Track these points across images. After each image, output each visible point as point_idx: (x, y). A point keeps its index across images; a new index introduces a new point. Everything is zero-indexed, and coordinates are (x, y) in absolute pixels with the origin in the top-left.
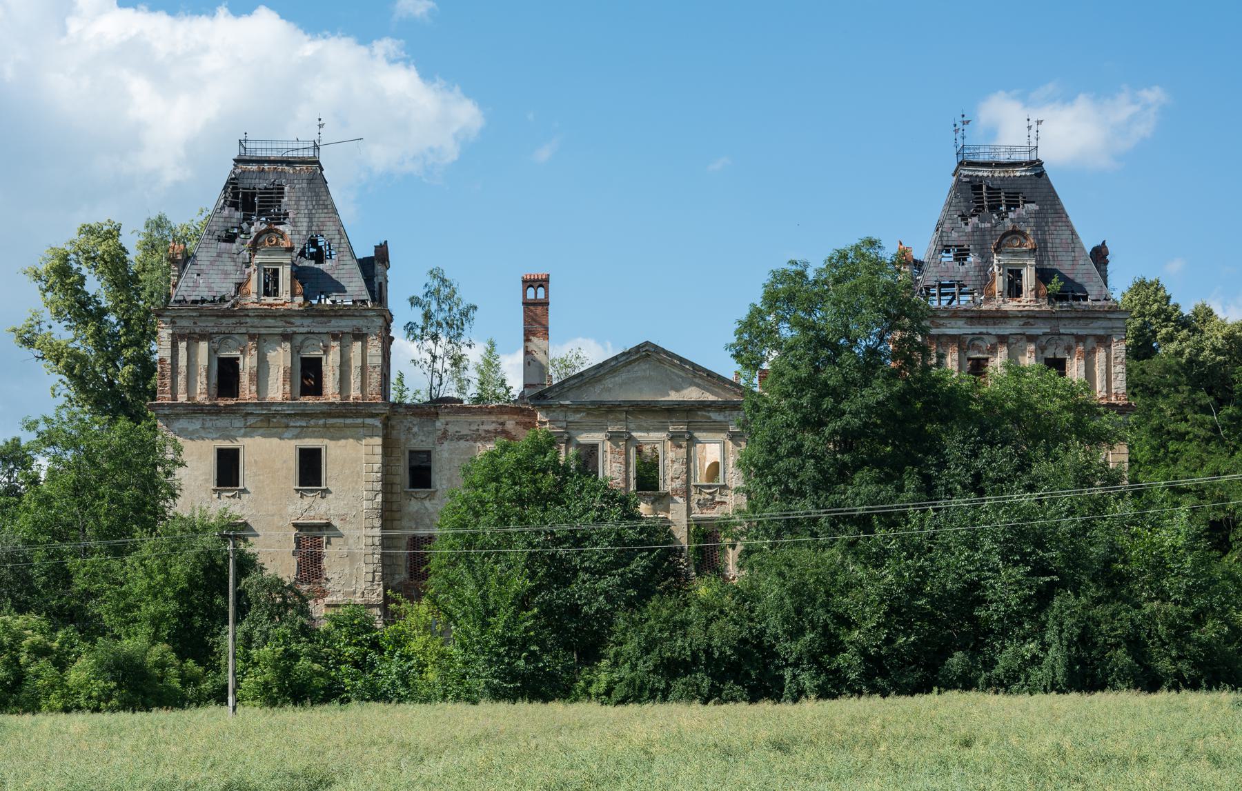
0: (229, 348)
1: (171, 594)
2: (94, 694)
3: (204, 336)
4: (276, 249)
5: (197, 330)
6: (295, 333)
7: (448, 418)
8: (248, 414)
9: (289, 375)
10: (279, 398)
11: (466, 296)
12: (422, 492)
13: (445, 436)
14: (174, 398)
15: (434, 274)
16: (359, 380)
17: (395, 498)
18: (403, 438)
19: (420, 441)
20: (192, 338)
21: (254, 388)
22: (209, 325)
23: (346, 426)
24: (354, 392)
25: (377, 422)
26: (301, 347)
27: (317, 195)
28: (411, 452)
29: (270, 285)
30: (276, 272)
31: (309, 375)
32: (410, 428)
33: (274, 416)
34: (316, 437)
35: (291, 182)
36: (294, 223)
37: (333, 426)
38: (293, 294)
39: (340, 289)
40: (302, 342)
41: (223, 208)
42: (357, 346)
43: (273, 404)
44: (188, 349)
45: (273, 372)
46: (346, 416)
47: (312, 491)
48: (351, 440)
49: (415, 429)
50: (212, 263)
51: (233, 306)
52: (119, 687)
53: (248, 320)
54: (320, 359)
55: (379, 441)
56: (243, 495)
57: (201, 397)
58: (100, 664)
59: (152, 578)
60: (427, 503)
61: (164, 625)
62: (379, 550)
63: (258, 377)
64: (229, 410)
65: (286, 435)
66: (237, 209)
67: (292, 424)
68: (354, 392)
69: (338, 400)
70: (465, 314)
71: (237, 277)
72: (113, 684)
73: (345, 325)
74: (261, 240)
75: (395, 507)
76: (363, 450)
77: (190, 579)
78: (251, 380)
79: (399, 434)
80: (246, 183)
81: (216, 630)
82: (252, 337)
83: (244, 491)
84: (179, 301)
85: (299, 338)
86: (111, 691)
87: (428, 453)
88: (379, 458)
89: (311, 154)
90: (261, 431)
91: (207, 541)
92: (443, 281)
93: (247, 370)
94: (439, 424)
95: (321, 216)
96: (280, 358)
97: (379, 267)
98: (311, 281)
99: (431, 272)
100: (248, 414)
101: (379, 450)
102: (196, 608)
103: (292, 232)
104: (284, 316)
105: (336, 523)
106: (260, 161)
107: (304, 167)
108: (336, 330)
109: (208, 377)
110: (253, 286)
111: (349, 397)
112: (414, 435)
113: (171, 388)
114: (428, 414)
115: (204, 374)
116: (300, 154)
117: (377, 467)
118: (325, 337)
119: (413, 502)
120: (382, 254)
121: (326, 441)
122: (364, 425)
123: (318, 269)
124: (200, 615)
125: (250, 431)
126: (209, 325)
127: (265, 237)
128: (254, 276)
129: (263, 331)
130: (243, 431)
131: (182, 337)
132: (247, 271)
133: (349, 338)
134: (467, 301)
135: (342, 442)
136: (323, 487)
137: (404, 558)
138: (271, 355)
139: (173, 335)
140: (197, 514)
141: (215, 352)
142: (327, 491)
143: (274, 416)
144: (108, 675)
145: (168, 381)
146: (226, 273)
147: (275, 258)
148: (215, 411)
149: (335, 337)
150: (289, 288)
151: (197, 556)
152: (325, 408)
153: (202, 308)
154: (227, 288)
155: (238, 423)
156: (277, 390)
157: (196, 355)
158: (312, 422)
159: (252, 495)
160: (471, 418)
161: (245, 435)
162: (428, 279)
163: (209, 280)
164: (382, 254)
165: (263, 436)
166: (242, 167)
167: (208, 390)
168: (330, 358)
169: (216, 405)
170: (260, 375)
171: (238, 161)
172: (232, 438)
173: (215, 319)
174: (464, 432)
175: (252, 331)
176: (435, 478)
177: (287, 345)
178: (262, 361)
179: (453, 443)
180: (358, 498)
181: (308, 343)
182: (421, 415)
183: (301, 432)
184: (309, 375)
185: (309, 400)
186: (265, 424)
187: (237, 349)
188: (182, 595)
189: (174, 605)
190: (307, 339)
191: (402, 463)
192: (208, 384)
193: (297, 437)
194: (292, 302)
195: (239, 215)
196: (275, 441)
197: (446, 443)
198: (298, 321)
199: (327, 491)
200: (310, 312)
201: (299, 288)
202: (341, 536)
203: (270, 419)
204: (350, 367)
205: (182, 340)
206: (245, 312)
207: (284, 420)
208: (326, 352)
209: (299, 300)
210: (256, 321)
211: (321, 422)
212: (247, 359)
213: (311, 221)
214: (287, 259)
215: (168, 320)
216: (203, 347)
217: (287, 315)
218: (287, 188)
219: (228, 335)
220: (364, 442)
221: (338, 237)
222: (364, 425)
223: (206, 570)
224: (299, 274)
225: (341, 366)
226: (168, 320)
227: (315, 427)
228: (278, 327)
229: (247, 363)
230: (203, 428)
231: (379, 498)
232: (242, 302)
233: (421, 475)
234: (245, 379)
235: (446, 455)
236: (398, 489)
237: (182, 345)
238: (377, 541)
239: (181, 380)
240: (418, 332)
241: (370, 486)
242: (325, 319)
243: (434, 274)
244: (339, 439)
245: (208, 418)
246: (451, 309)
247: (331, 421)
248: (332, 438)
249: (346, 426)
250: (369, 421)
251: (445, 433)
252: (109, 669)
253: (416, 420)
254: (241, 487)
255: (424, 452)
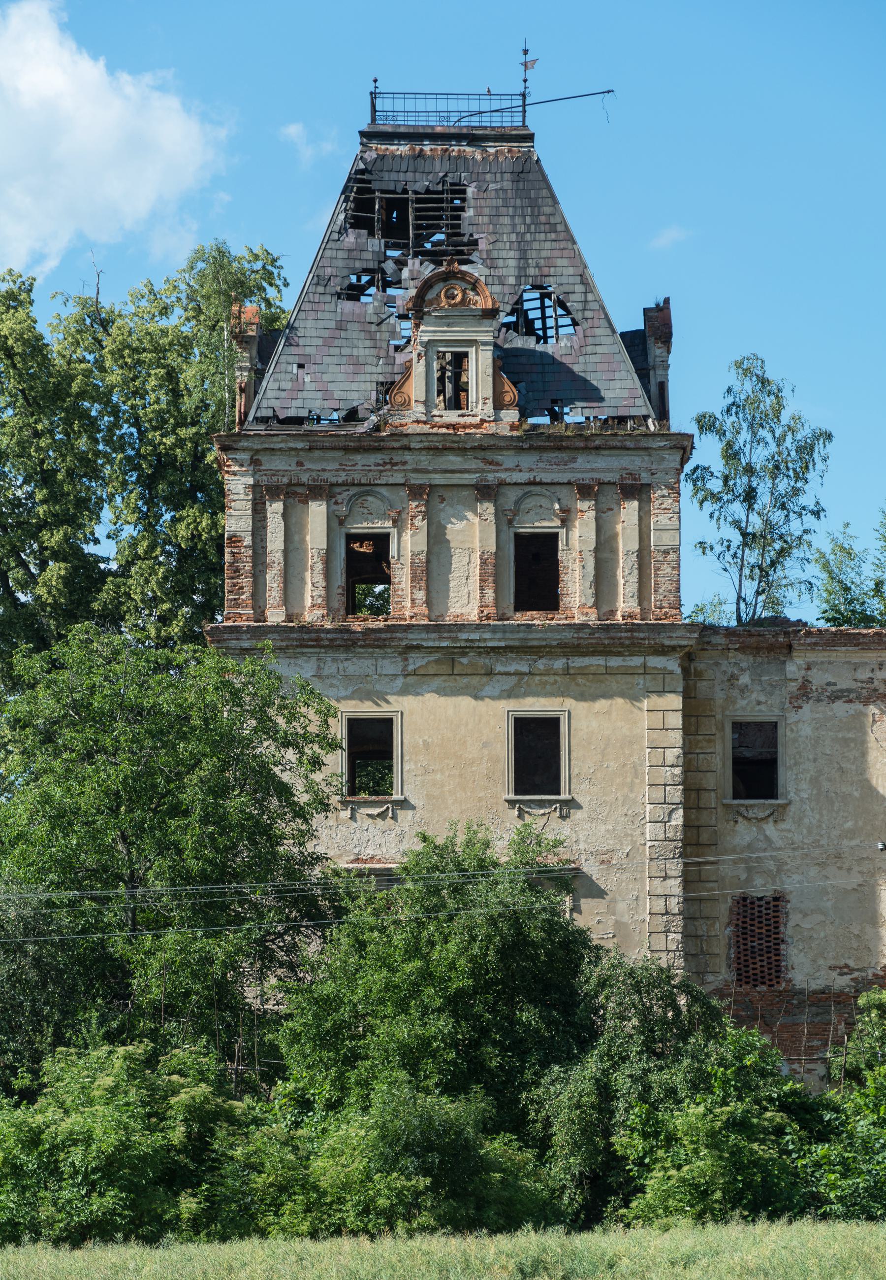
0: (370, 515)
1: (438, 1002)
2: (382, 1202)
3: (317, 491)
4: (462, 312)
5: (305, 478)
6: (502, 484)
7: (812, 657)
8: (411, 648)
9: (491, 571)
10: (472, 615)
11: (806, 408)
12: (758, 807)
13: (804, 691)
14: (260, 616)
15: (744, 368)
16: (634, 578)
17: (705, 818)
18: (719, 696)
19: (754, 703)
20: (295, 494)
21: (421, 595)
22: (329, 467)
23: (609, 672)
24: (625, 603)
25: (673, 664)
26: (516, 513)
27: (534, 204)
28: (739, 727)
29: (452, 386)
30: (459, 359)
31: (533, 571)
32: (733, 678)
33: (463, 651)
34: (547, 695)
35: (478, 178)
36: (490, 262)
37: (583, 672)
38: (499, 405)
39: (592, 394)
40: (518, 503)
41: (342, 231)
42: (631, 508)
43: (462, 627)
44: (285, 516)
45: (458, 561)
46: (617, 651)
47: (541, 804)
48: (620, 701)
49: (745, 679)
50: (328, 343)
51: (377, 428)
52: (433, 1188)
53: (408, 457)
54: (554, 537)
55: (675, 701)
56: (400, 813)
57: (312, 615)
58: (386, 1136)
59: (393, 970)
60: (770, 829)
61: (429, 1065)
62: (679, 921)
63: (428, 572)
64: (374, 641)
65: (488, 690)
66: (371, 234)
67: (499, 668)
68: (625, 603)
69: (592, 618)
70: (806, 450)
71: (378, 371)
72: (424, 1182)
73: (605, 466)
74: (430, 296)
75: (705, 837)
76: (645, 720)
77: (477, 970)
78: (414, 578)
79: (713, 688)
80: (389, 180)
81: (528, 1075)
82: (416, 492)
83: (404, 804)
84: (264, 420)
85: (511, 496)
86: (418, 1194)
87: (775, 725)
88: (677, 738)
89: (518, 120)
90: (437, 682)
91: (505, 893)
92: (764, 381)
93: (407, 558)
94: (794, 668)
95: (543, 246)
96: (473, 535)
97: (656, 350)
98: (534, 379)
99: (738, 365)
100: (411, 648)
101: (676, 720)
102: (484, 1032)
103: (493, 274)
104: (482, 448)
105: (591, 868)
106: (414, 136)
107: (505, 147)
108: (586, 478)
109: (327, 574)
110: (416, 388)
111: (613, 612)
112: (744, 690)
113: (254, 596)
114: (771, 648)
115: (319, 566)
116: (496, 121)
117: (672, 755)
118: (563, 492)
119: (742, 826)
120: (658, 325)
121: (569, 703)
122: (645, 671)
123: (544, 355)
124: (495, 1043)
125: (414, 683)
126: (329, 467)
127: (440, 289)
128: (419, 369)
129: (438, 479)
130: (400, 682)
131: (274, 492)
132: (400, 358)
133: (613, 493)
134: (814, 421)
135: (602, 704)
136: (564, 796)
137: (724, 942)
138: (455, 529)
139: (255, 487)
140: (461, 839)
141: (341, 523)
142: (571, 804)
143: (463, 651)
144: (409, 1162)
145: (246, 582)
146: (357, 364)
147: (459, 332)
148: (344, 642)
149: (585, 491)
150: (489, 393)
151: (492, 921)
152: (568, 635)
153: (311, 433)
154: (361, 392)
155: (390, 666)
156: (468, 598)
157: (302, 528)
158: (541, 664)
159: (419, 812)
160: (856, 656)
161: (404, 691)
162: (732, 378)
163: (319, 382)
164: (658, 325)
165: (442, 692)
166: (379, 148)
167: (328, 598)
168: (576, 533)
169: (347, 630)
170: (433, 569)
171: (367, 136)
172: (380, 697)
173: (347, 456)
174: (844, 684)
175: (417, 479)
176: (786, 777)
177: (488, 508)
178: (437, 541)
179: (822, 707)
180: (636, 819)
181: (530, 503)
182: (756, 650)
183: (518, 685)
184: (533, 571)
185: (535, 618)
186: (445, 669)
187: (384, 516)
188: (456, 1004)
189: (442, 1024)
190: (526, 495)
191: (719, 748)
192: (327, 588)
193: (509, 694)
194: (497, 420)
195: (376, 244)
196: (465, 702)
197: (807, 707)
198: (508, 459)
199: (571, 804)
200: (530, 442)
201: (510, 393)
202: (600, 893)
203: (453, 657)
204: (614, 551)
205: (274, 497)
206: (402, 442)
207: (484, 661)
208: (566, 522)
209: (511, 416)
210: (424, 460)
211: (559, 664)
212: (407, 537)
213: (523, 257)
214: (485, 333)
215: (245, 456)
216: (317, 513)
217: (487, 448)
218: (470, 191)
219: (366, 489)
220: (645, 704)
221: (579, 288)
222: (645, 671)
223: (504, 953)
224: (507, 363)
225: (597, 550)
226: (245, 456)
227: (547, 673)
228: (468, 470)
229: (408, 546)
230: (318, 676)
231: (678, 819)
232: (395, 420)
233: (756, 772)
234: (402, 575)
235: (806, 730)
236: (710, 800)
237: (274, 510)
238: (674, 905)
239: (273, 579)
240: (715, 485)
241: (658, 794)
242: (564, 455)
243: (744, 368)
244: (594, 698)
245: (329, 656)
246: (780, 441)
247: (578, 662)
248: (581, 697)
249: (609, 672)
250: (655, 662)
251: (805, 686)
252: (407, 1148)
253: (745, 661)
254: (397, 796)
255: (760, 725)
